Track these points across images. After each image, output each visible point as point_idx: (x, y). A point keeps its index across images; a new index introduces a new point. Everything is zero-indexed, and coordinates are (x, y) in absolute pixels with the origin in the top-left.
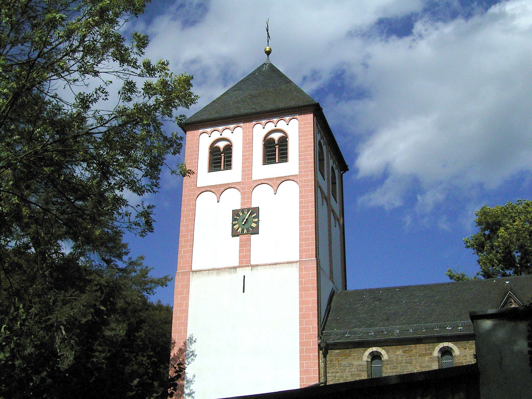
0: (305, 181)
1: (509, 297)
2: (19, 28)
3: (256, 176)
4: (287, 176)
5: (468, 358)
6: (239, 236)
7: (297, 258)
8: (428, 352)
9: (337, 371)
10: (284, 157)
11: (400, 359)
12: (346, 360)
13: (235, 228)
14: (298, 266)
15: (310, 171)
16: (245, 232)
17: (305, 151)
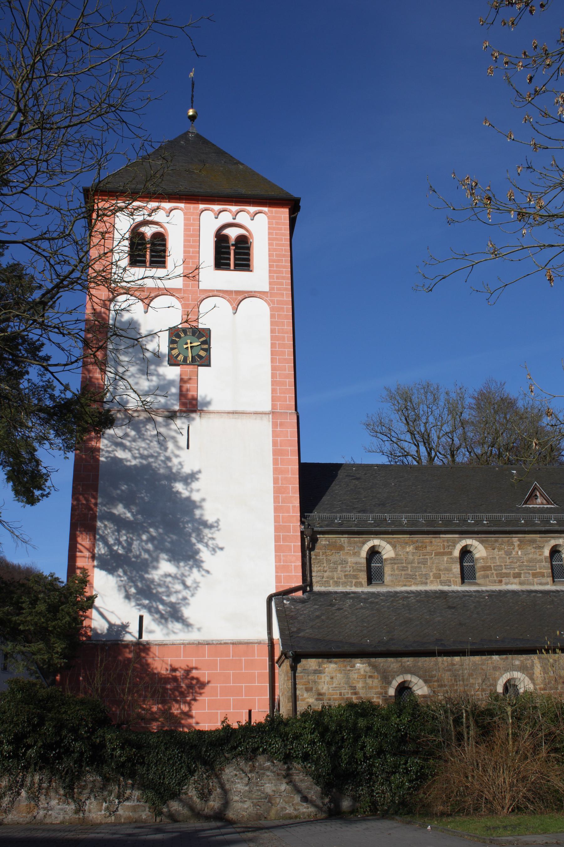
0: (279, 302)
1: (535, 489)
4: (251, 292)
5: (497, 561)
6: (178, 365)
7: (268, 408)
8: (446, 550)
9: (325, 569)
11: (411, 557)
12: (337, 555)
14: (271, 420)
15: (286, 289)
17: (278, 261)
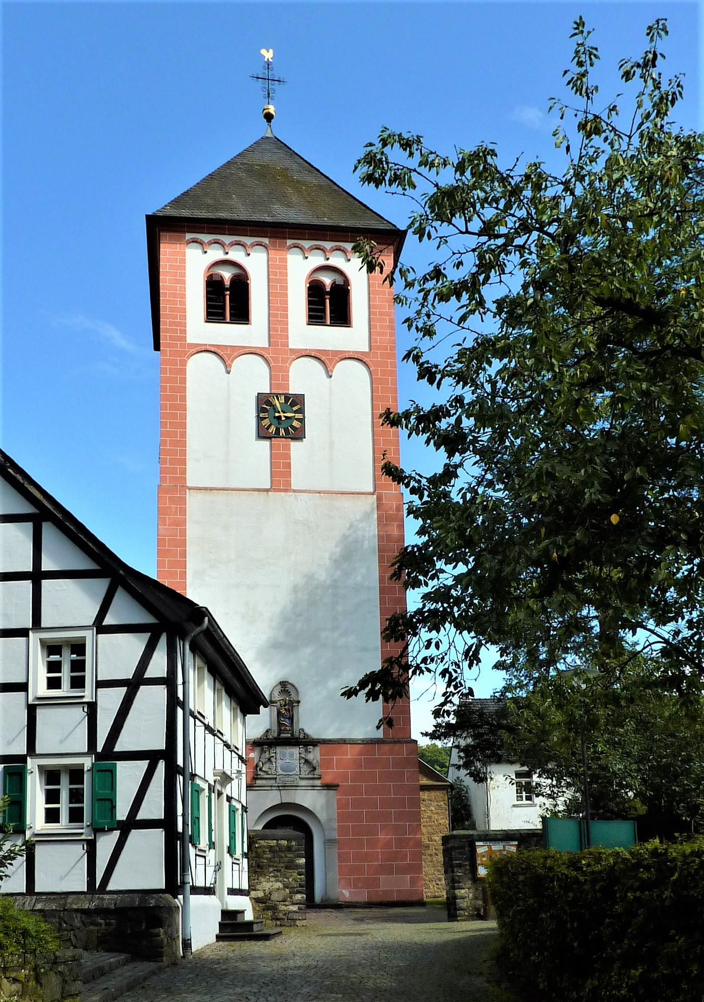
2: (565, 266)
3: (295, 342)
10: (315, 317)
13: (264, 425)
16: (281, 434)
